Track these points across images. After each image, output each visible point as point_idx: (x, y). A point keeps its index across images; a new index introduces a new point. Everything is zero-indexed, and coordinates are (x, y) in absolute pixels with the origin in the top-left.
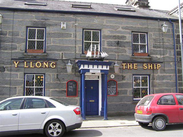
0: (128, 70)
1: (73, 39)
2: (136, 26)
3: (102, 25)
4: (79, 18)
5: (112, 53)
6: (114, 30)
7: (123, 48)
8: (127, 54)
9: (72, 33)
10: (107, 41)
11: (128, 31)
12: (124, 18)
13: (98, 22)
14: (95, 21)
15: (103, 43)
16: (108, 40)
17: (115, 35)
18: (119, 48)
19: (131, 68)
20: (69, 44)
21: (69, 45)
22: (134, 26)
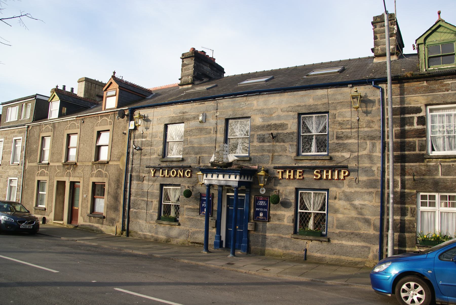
3: (252, 110)
7: (282, 144)
14: (241, 106)
18: (274, 143)
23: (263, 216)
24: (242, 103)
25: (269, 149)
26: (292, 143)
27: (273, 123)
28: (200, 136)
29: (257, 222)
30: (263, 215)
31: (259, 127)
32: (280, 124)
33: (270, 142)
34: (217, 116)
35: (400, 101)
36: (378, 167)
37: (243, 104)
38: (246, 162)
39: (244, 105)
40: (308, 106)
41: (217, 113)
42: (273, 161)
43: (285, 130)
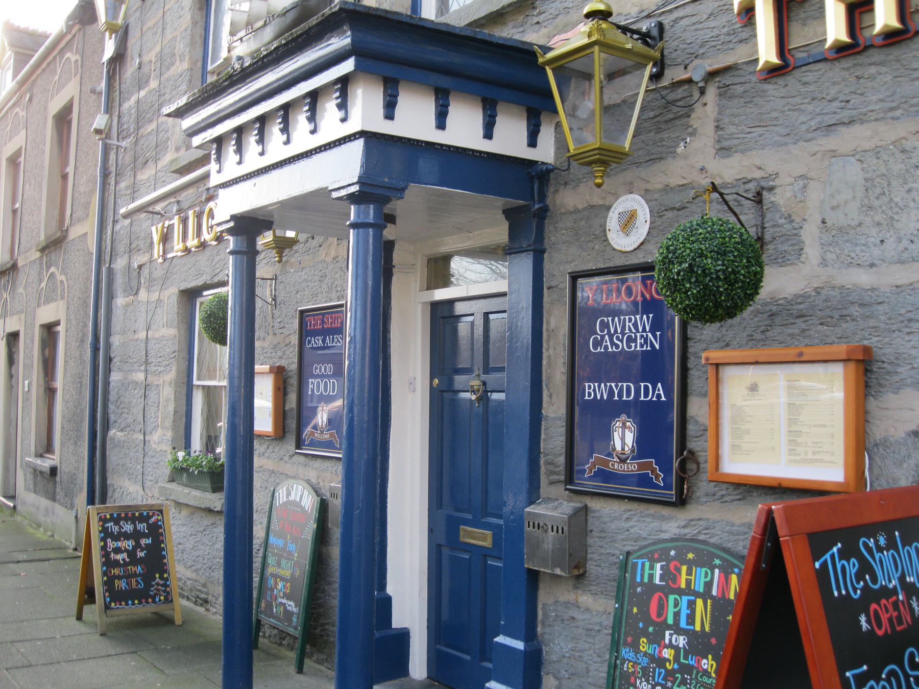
23: (644, 447)
24: (119, 557)
29: (595, 504)
30: (640, 440)
35: (540, 125)
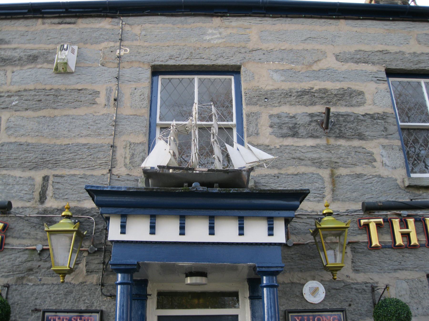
0: (395, 253)
1: (102, 113)
2: (403, 48)
3: (243, 51)
4: (137, 30)
5: (302, 169)
6: (299, 67)
7: (356, 143)
8: (385, 172)
9: (102, 88)
10: (271, 116)
11: (369, 68)
12: (342, 22)
13: (220, 41)
14: (208, 38)
15: (249, 123)
16: (275, 111)
17: (306, 85)
18: (332, 141)
19: (414, 240)
20: (85, 132)
21: (83, 141)
22: (393, 49)
25: (315, 156)
26: (387, 141)
27: (316, 88)
28: (52, 111)
31: (274, 93)
32: (339, 90)
33: (317, 137)
34: (119, 57)
36: (103, 294)
37: (213, 34)
38: (422, 131)
39: (216, 36)
40: (409, 54)
41: (120, 49)
42: (337, 193)
43: (359, 106)
